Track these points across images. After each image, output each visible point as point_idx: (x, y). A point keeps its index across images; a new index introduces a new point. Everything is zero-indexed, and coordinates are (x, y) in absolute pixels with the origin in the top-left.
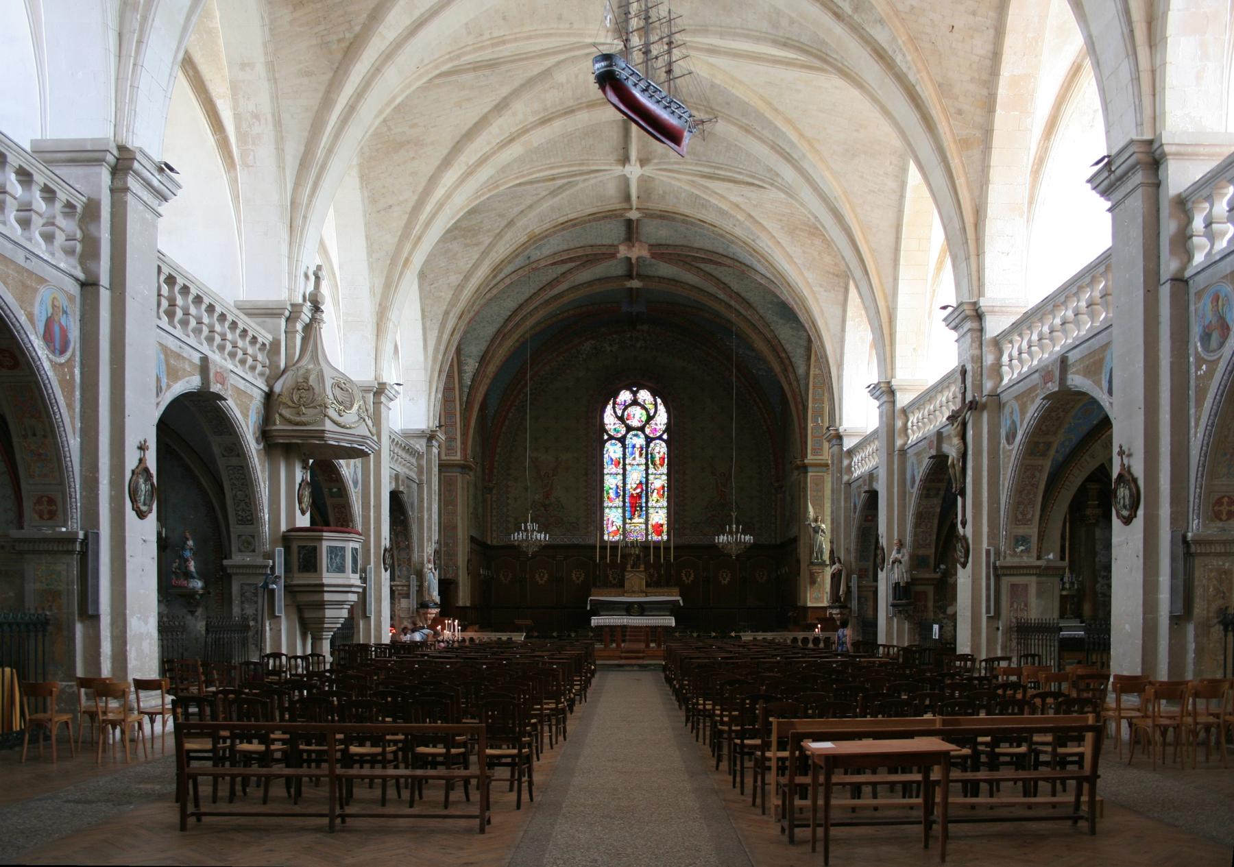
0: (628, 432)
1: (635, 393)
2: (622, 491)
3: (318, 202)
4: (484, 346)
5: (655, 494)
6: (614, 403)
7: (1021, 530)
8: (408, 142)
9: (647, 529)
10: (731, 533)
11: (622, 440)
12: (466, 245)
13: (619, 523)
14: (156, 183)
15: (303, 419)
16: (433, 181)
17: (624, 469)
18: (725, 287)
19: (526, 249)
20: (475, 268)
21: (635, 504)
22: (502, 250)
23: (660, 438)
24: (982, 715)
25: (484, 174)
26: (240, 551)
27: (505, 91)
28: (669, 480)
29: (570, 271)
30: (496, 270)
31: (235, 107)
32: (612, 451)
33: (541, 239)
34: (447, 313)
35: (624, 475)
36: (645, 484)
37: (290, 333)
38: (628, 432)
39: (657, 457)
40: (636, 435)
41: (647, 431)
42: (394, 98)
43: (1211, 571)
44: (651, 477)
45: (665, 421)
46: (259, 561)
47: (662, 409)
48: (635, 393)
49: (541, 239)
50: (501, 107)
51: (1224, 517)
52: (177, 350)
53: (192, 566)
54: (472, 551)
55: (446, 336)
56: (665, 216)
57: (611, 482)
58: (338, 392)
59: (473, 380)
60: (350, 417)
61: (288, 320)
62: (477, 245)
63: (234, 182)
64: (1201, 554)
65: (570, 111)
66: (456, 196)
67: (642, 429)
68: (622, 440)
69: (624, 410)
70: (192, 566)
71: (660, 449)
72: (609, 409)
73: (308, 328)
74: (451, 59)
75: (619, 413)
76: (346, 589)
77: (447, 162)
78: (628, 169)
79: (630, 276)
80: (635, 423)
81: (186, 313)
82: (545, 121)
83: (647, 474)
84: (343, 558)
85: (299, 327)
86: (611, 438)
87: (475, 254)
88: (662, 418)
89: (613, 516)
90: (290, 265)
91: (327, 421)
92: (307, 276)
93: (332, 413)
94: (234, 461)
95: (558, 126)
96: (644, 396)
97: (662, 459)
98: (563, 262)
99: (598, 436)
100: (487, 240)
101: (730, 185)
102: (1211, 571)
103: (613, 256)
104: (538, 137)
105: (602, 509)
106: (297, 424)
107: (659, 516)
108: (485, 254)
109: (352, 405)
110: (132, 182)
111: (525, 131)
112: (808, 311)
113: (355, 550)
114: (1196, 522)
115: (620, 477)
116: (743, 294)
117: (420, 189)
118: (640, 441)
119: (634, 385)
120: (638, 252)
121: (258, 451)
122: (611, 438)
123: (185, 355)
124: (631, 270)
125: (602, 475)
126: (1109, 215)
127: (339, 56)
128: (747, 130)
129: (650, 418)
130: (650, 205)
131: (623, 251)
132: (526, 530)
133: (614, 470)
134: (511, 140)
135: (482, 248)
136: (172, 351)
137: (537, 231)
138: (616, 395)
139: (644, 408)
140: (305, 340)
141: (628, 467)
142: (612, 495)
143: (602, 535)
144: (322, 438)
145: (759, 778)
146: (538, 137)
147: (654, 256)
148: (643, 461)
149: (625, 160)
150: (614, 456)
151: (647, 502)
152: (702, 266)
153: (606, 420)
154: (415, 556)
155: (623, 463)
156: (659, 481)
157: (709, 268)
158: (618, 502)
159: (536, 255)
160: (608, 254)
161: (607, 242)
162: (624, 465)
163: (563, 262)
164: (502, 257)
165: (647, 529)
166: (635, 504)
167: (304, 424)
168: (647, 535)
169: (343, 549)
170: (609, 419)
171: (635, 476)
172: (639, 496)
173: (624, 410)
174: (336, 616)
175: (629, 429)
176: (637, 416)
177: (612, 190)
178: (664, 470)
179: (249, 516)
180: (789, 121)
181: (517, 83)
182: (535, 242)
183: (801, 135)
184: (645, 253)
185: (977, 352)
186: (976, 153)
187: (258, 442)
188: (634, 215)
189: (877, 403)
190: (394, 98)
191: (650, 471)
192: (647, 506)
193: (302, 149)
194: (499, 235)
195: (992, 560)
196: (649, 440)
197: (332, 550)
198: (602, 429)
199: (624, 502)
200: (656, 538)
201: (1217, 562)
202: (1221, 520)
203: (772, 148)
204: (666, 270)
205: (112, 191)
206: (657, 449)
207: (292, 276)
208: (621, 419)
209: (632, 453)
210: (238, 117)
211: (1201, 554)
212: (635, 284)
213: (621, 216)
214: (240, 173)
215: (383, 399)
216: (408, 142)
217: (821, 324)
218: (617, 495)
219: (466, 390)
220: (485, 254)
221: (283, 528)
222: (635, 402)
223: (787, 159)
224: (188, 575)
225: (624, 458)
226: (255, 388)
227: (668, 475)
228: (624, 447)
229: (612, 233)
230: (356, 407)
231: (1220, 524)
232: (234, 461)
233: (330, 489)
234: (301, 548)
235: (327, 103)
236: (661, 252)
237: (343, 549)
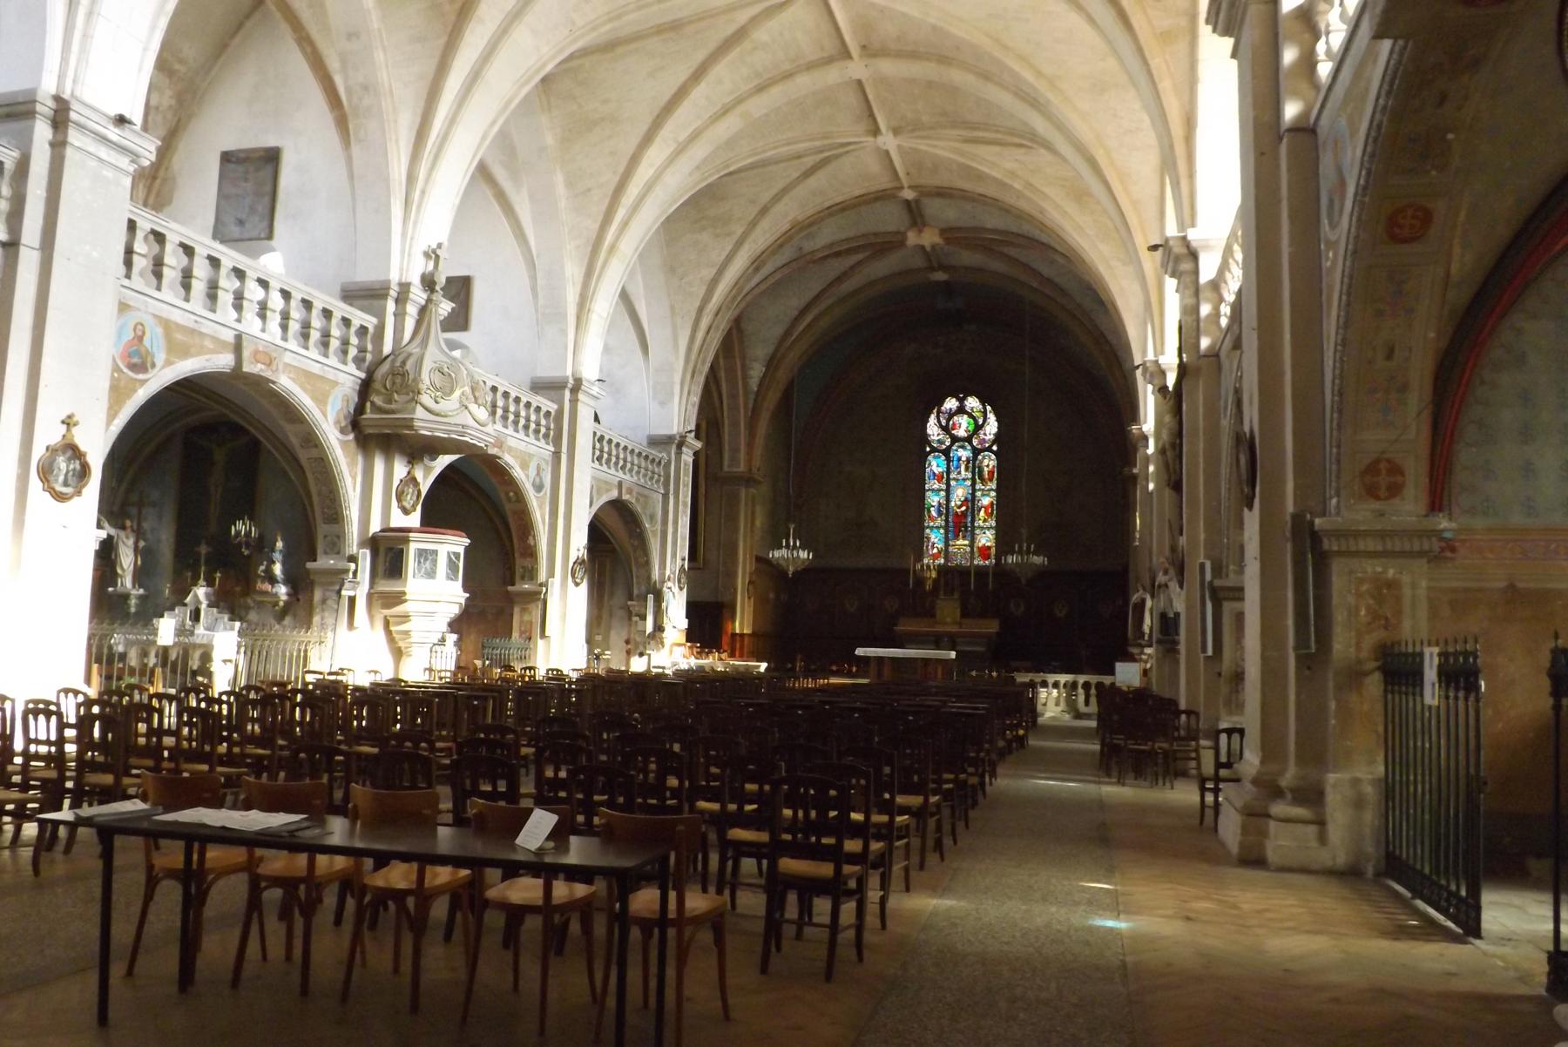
0: (952, 444)
1: (961, 401)
2: (945, 509)
4: (771, 349)
5: (982, 513)
6: (939, 412)
8: (603, 119)
9: (972, 552)
10: (1020, 552)
11: (946, 452)
12: (717, 236)
13: (941, 545)
14: (114, 138)
15: (393, 406)
16: (634, 160)
17: (948, 485)
18: (1036, 273)
19: (791, 238)
20: (728, 262)
21: (960, 524)
22: (761, 239)
23: (989, 449)
24: (308, 781)
25: (700, 151)
26: (326, 553)
27: (700, 56)
28: (998, 497)
29: (859, 263)
30: (757, 263)
31: (346, 79)
32: (936, 465)
33: (810, 225)
34: (701, 310)
35: (948, 491)
36: (971, 501)
38: (952, 444)
40: (963, 447)
41: (975, 442)
42: (544, 65)
43: (1362, 581)
44: (978, 494)
45: (995, 430)
46: (341, 564)
47: (992, 418)
48: (961, 401)
49: (810, 225)
50: (698, 75)
51: (1383, 493)
52: (192, 325)
53: (278, 569)
54: (757, 571)
55: (700, 335)
56: (942, 193)
57: (933, 499)
58: (437, 378)
59: (760, 385)
60: (449, 404)
61: (397, 301)
62: (729, 235)
63: (349, 160)
64: (1339, 553)
65: (788, 76)
66: (666, 178)
67: (969, 439)
68: (946, 452)
69: (948, 421)
70: (278, 569)
71: (989, 462)
72: (932, 419)
74: (610, 20)
75: (944, 422)
77: (647, 139)
78: (880, 139)
79: (932, 269)
80: (961, 433)
82: (760, 89)
83: (974, 490)
86: (934, 450)
88: (992, 427)
89: (936, 538)
91: (419, 408)
93: (426, 399)
94: (314, 453)
95: (776, 95)
96: (972, 403)
97: (991, 473)
98: (850, 251)
100: (739, 231)
101: (997, 149)
102: (1362, 581)
103: (901, 243)
104: (758, 106)
105: (923, 529)
106: (387, 412)
107: (986, 539)
108: (739, 244)
109: (452, 391)
111: (739, 101)
112: (1107, 290)
114: (1334, 501)
115: (943, 494)
116: (1057, 280)
117: (621, 169)
118: (965, 454)
119: (961, 393)
120: (929, 238)
121: (343, 444)
122: (934, 450)
123: (204, 330)
124: (932, 258)
125: (924, 491)
126: (1235, 63)
127: (453, 17)
128: (986, 77)
129: (978, 428)
130: (922, 182)
131: (912, 238)
132: (788, 546)
133: (936, 486)
134: (725, 111)
135: (735, 238)
136: (177, 325)
137: (800, 218)
138: (941, 403)
139: (971, 416)
140: (419, 323)
141: (953, 483)
142: (934, 514)
144: (411, 427)
145: (730, 863)
146: (758, 106)
147: (948, 241)
148: (969, 475)
149: (876, 131)
150: (937, 470)
151: (973, 521)
152: (1006, 250)
153: (929, 431)
154: (656, 575)
155: (945, 477)
157: (1012, 252)
158: (940, 522)
159: (809, 246)
160: (893, 242)
161: (891, 228)
162: (948, 479)
163: (850, 251)
164: (763, 247)
165: (972, 552)
166: (960, 524)
167: (393, 412)
168: (972, 558)
169: (435, 552)
170: (933, 429)
171: (959, 494)
172: (964, 514)
173: (948, 421)
175: (955, 439)
176: (963, 425)
177: (874, 166)
178: (993, 485)
179: (335, 516)
180: (1022, 58)
181: (712, 45)
182: (801, 230)
183: (1039, 74)
184: (938, 240)
185: (1191, 301)
186: (1182, 46)
187: (343, 431)
188: (909, 194)
190: (544, 65)
191: (978, 487)
192: (973, 527)
193: (418, 120)
194: (753, 224)
195: (1208, 577)
196: (976, 452)
197: (422, 553)
198: (925, 439)
199: (947, 521)
200: (978, 561)
201: (1373, 567)
202: (1377, 498)
203: (1016, 94)
204: (968, 258)
205: (53, 145)
206: (986, 462)
208: (946, 429)
209: (958, 467)
210: (349, 90)
211: (1339, 553)
212: (940, 276)
213: (894, 197)
214: (356, 149)
216: (603, 119)
217: (1120, 303)
218: (940, 513)
219: (752, 396)
222: (961, 410)
223: (1032, 105)
224: (272, 580)
225: (948, 472)
226: (347, 377)
227: (998, 490)
228: (949, 460)
229: (889, 219)
230: (457, 393)
231: (1376, 505)
232: (314, 453)
233: (507, 494)
235: (442, 68)
236: (952, 234)
237: (435, 552)
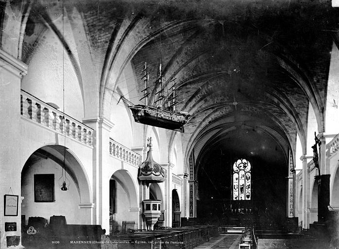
3: (174, 142)
7: (11, 220)
23: (249, 172)
32: (235, 176)
37: (144, 154)
39: (248, 177)
44: (246, 183)
47: (249, 164)
57: (235, 183)
58: (155, 167)
71: (249, 175)
72: (235, 165)
73: (148, 152)
76: (157, 214)
81: (130, 158)
84: (156, 207)
85: (146, 152)
87: (195, 128)
89: (236, 193)
90: (100, 109)
92: (148, 140)
97: (249, 178)
99: (232, 172)
110: (103, 125)
113: (159, 205)
119: (241, 158)
122: (235, 173)
143: (233, 199)
156: (249, 183)
174: (154, 221)
189: (302, 161)
205: (99, 127)
207: (145, 140)
215: (170, 167)
220: (198, 127)
221: (143, 200)
234: (146, 205)
